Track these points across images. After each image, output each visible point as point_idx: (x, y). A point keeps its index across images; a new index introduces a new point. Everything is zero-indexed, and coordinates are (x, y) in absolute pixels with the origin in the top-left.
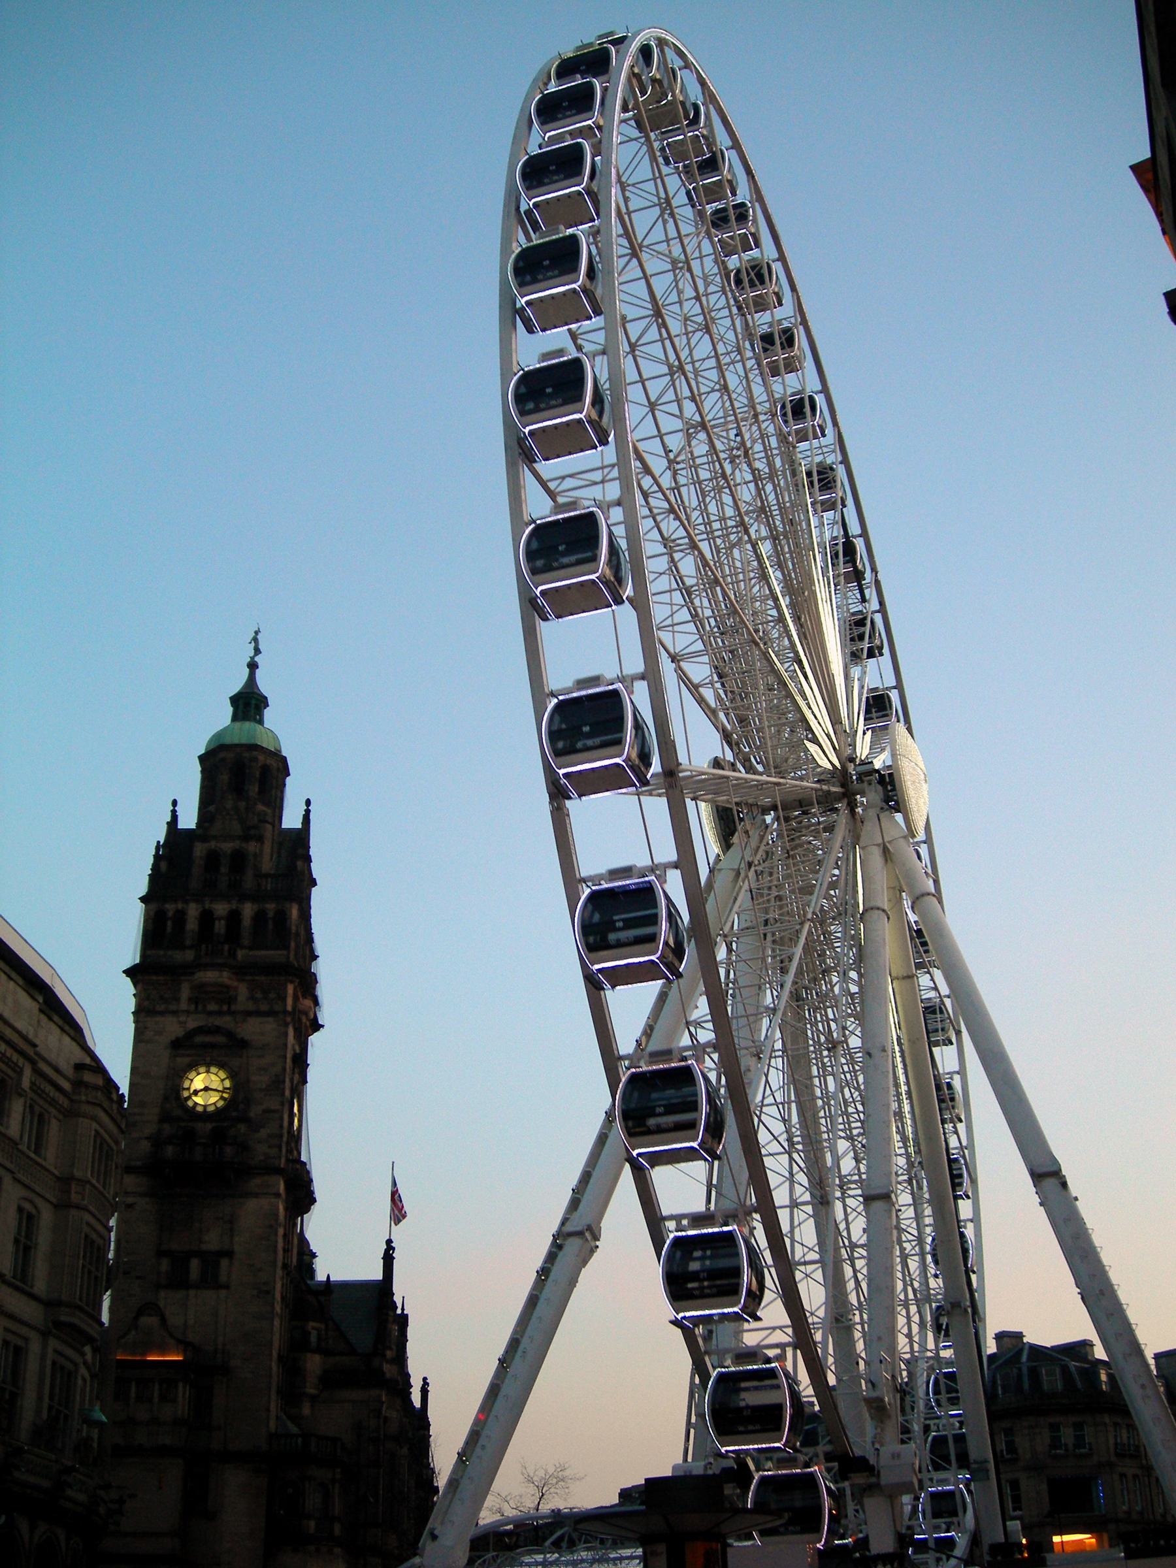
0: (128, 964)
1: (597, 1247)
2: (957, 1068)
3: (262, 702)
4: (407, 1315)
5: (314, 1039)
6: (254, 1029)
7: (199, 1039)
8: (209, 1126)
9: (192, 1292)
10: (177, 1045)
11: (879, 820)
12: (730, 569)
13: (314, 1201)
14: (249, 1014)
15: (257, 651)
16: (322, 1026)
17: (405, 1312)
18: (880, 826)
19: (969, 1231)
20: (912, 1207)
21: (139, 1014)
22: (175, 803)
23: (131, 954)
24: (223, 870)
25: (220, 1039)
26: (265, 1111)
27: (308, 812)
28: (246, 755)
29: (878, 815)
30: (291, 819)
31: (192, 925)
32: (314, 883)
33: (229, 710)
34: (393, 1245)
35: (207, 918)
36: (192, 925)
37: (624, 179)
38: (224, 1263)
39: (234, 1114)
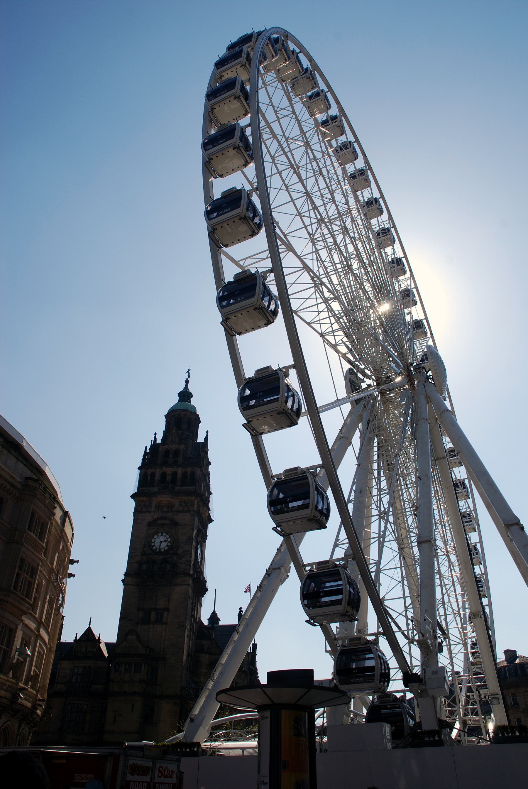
0: (132, 493)
1: (288, 576)
2: (478, 541)
3: (190, 395)
4: (256, 644)
5: (210, 526)
6: (183, 518)
7: (159, 522)
8: (161, 557)
9: (152, 626)
10: (150, 524)
11: (424, 386)
12: (353, 283)
13: (207, 590)
14: (179, 512)
15: (189, 377)
16: (213, 520)
17: (256, 643)
18: (425, 388)
19: (487, 610)
20: (327, 188)
21: (136, 512)
22: (155, 434)
23: (134, 489)
24: (171, 456)
25: (168, 522)
26: (184, 551)
27: (207, 435)
28: (182, 413)
29: (424, 384)
30: (200, 439)
31: (157, 477)
32: (210, 464)
33: (177, 398)
34: (242, 610)
35: (164, 475)
36: (157, 477)
37: (299, 118)
38: (165, 613)
39: (172, 552)
